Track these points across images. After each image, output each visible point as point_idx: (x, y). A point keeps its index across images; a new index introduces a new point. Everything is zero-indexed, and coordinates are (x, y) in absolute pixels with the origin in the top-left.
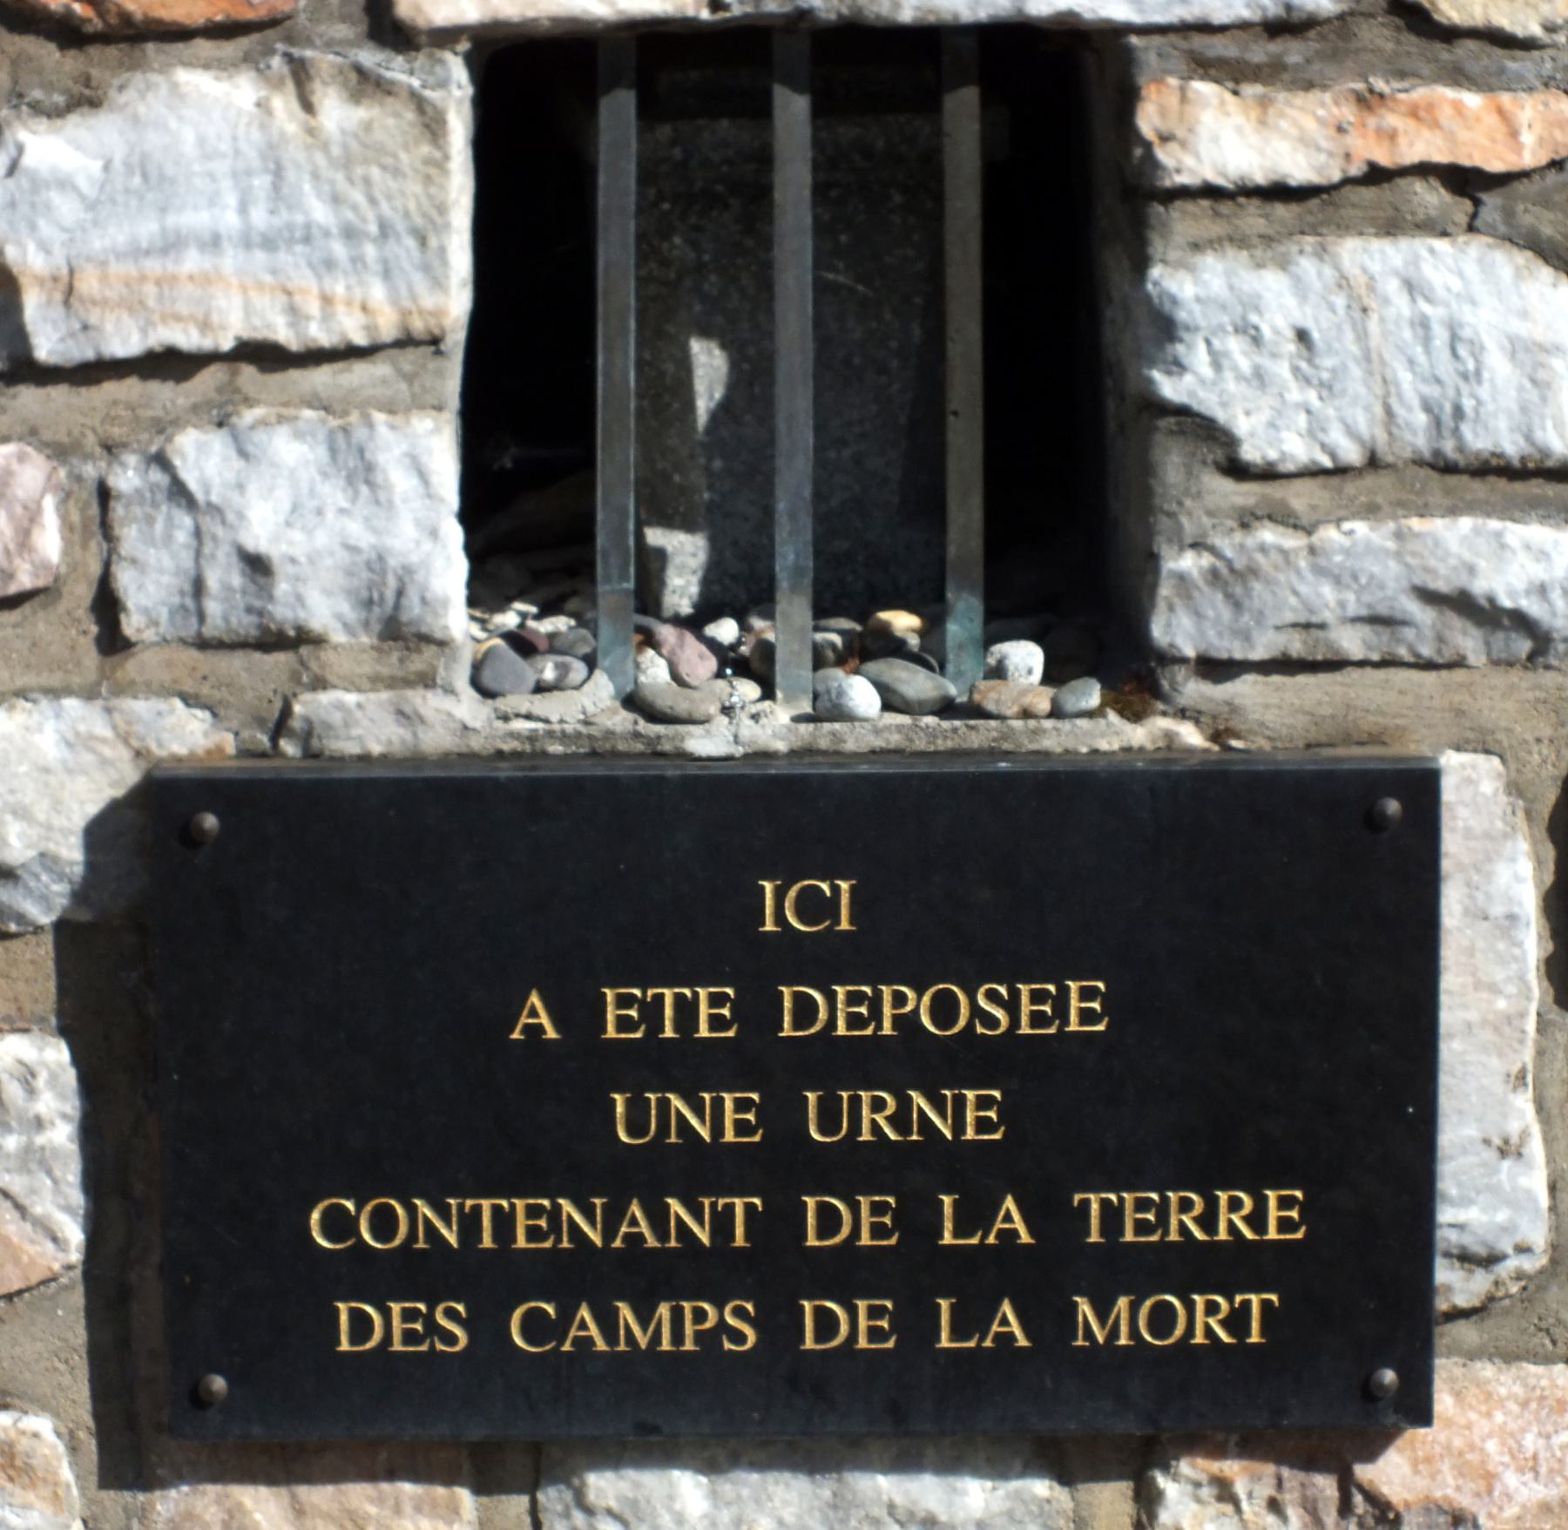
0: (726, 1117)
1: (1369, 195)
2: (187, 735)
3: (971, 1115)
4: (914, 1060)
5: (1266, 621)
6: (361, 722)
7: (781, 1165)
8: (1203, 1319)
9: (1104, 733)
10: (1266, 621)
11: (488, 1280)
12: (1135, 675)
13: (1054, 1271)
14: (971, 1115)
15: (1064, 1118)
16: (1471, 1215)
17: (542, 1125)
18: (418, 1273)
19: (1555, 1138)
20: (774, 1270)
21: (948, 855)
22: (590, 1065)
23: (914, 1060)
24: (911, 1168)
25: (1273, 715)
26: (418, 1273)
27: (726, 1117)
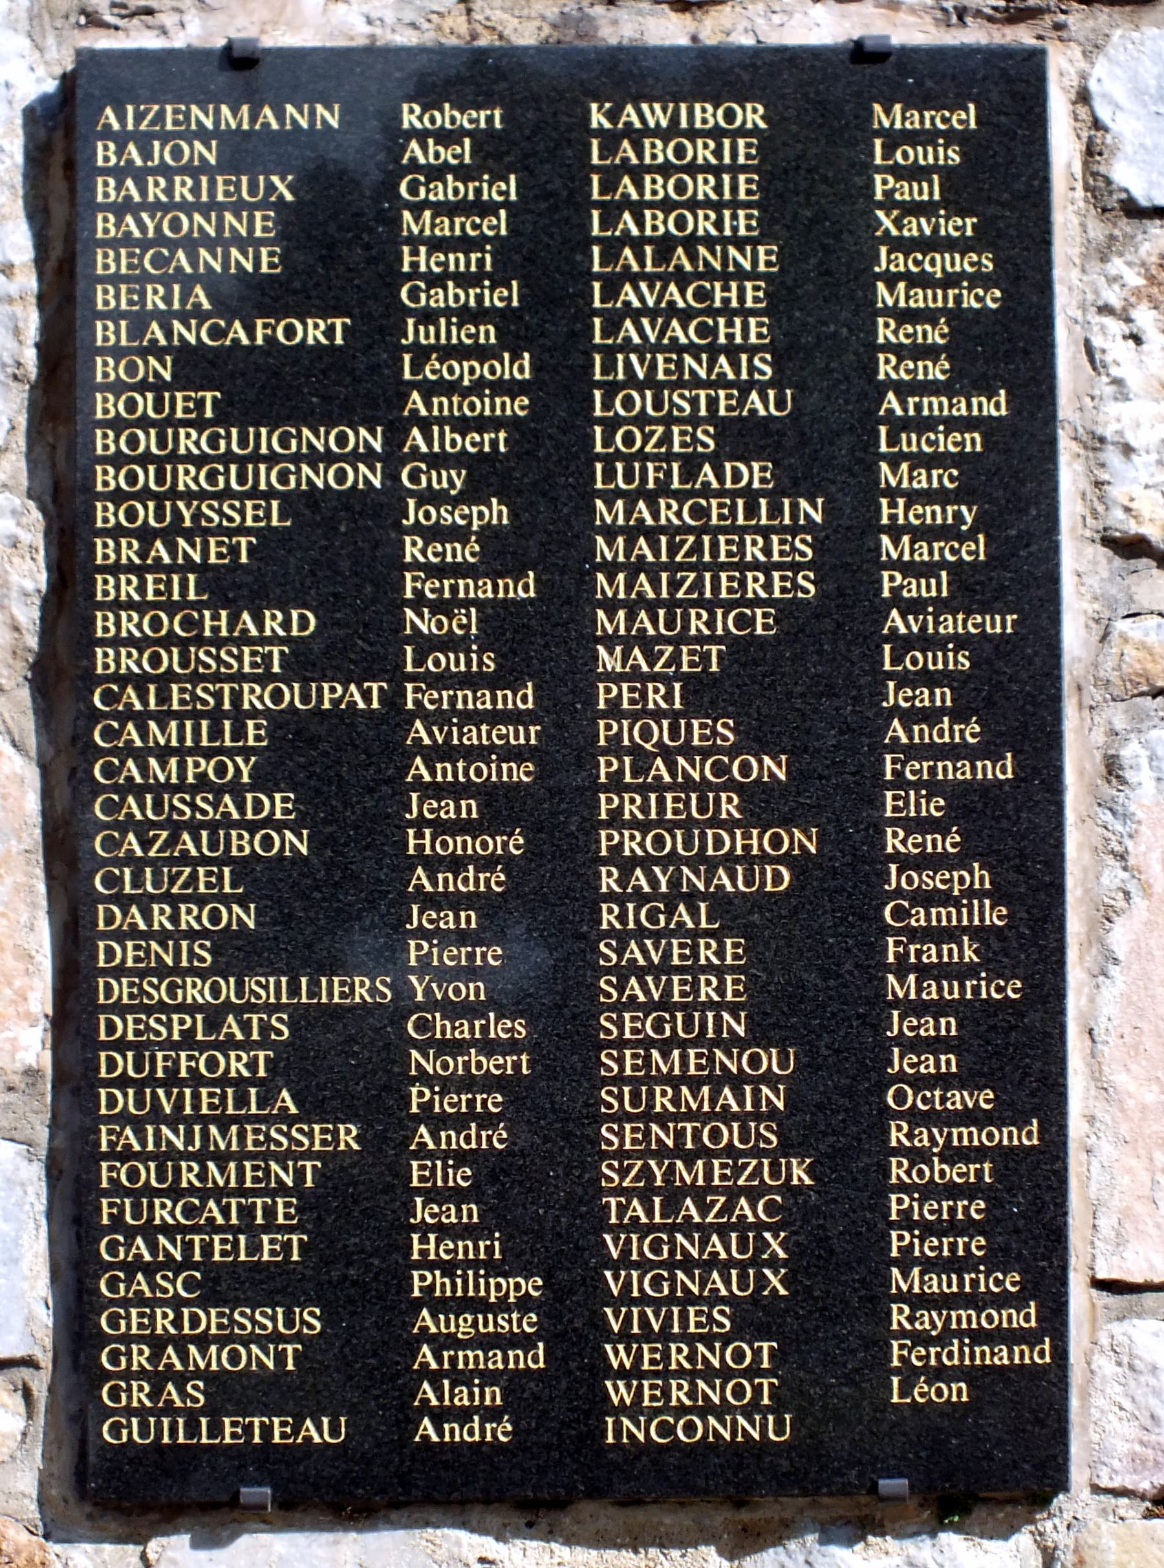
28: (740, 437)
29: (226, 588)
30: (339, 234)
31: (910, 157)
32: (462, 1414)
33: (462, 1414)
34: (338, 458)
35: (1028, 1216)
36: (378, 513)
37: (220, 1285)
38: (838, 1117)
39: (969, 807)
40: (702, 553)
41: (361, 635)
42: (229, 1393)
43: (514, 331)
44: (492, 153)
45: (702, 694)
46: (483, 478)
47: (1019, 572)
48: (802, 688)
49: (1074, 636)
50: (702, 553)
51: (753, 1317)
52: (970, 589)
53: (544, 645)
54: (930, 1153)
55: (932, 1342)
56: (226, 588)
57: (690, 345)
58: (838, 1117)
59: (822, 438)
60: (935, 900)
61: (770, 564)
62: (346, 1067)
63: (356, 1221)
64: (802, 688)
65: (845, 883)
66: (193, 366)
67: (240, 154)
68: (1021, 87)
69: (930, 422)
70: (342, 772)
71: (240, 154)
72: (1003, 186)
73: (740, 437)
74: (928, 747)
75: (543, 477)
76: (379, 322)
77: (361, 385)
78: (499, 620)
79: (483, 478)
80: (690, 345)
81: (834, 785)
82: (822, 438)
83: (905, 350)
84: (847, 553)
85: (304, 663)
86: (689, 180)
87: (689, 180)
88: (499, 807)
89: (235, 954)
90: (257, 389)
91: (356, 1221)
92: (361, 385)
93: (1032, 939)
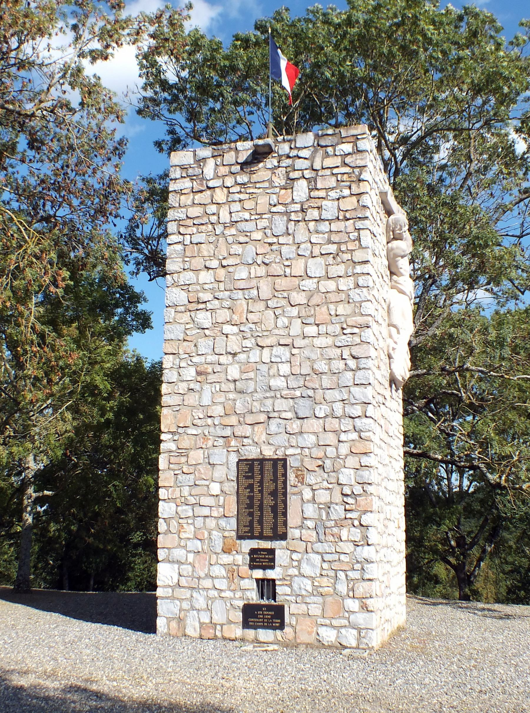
0: (262, 616)
1: (283, 585)
2: (246, 602)
3: (269, 617)
4: (268, 615)
5: (280, 599)
6: (251, 602)
7: (263, 618)
8: (277, 624)
9: (275, 604)
10: (280, 599)
11: (254, 622)
12: (275, 601)
13: (272, 623)
14: (269, 617)
15: (273, 617)
16: (362, 144)
17: (256, 616)
18: (252, 622)
19: (274, 493)
20: (263, 622)
21: (269, 608)
22: (257, 614)
23: (268, 615)
24: (268, 618)
25: (280, 603)
26: (252, 622)
27: (262, 616)
28: (271, 480)
29: (245, 488)
30: (251, 469)
31: (280, 463)
32: (256, 534)
33: (256, 534)
34: (251, 481)
35: (285, 523)
36: (253, 484)
37: (245, 526)
38: (275, 517)
39: (282, 500)
40: (269, 486)
41: (252, 491)
42: (245, 532)
43: (260, 474)
44: (259, 464)
45: (269, 494)
46: (258, 482)
47: (285, 488)
48: (274, 493)
49: (288, 491)
50: (269, 486)
51: (271, 529)
52: (283, 488)
53: (261, 491)
54: (280, 519)
55: (280, 530)
56: (245, 488)
57: (268, 475)
58: (275, 517)
59: (275, 480)
60: (281, 506)
61: (272, 487)
62: (251, 514)
63: (251, 522)
64: (274, 509)
65: (276, 505)
66: (244, 476)
67: (247, 464)
68: (140, 31)
69: (281, 479)
70: (251, 498)
71: (247, 464)
72: (285, 466)
73: (271, 480)
74: (280, 497)
75: (261, 482)
76: (253, 474)
77: (252, 477)
78: (259, 490)
79: (258, 482)
80: (268, 475)
81: (275, 499)
82: (275, 480)
83: (279, 475)
84: (276, 486)
85: (249, 492)
86: (268, 466)
87: (268, 466)
88: (259, 500)
89: (246, 508)
90: (247, 477)
91: (251, 522)
92: (252, 477)
93: (286, 508)
